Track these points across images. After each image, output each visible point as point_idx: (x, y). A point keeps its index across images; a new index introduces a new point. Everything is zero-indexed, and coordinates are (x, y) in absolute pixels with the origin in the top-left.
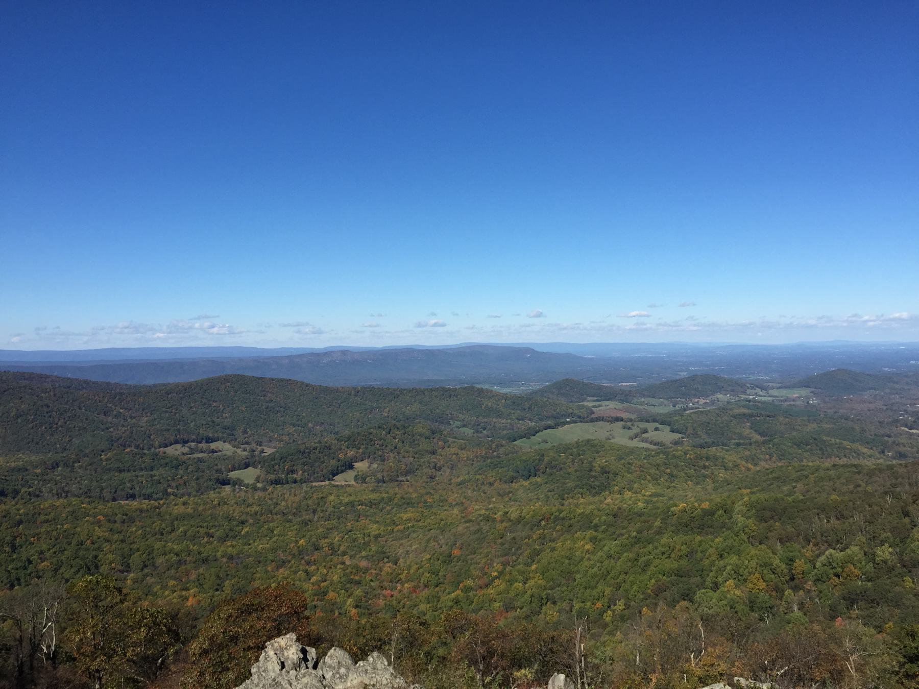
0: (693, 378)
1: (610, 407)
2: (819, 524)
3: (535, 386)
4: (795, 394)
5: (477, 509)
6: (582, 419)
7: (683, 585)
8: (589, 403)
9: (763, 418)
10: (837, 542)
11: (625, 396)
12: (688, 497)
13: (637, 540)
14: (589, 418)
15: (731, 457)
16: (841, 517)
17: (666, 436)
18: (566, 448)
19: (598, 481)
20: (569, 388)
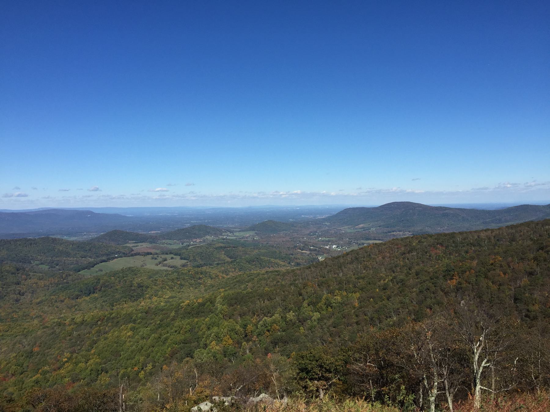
0: (193, 227)
1: (143, 247)
2: (260, 304)
3: (94, 235)
4: (247, 234)
5: (51, 319)
6: (125, 255)
7: (186, 349)
8: (130, 245)
9: (231, 249)
11: (153, 240)
12: (191, 296)
13: (160, 326)
14: (131, 254)
15: (214, 271)
16: (270, 299)
17: (178, 262)
18: (115, 274)
19: (136, 292)
20: (116, 236)
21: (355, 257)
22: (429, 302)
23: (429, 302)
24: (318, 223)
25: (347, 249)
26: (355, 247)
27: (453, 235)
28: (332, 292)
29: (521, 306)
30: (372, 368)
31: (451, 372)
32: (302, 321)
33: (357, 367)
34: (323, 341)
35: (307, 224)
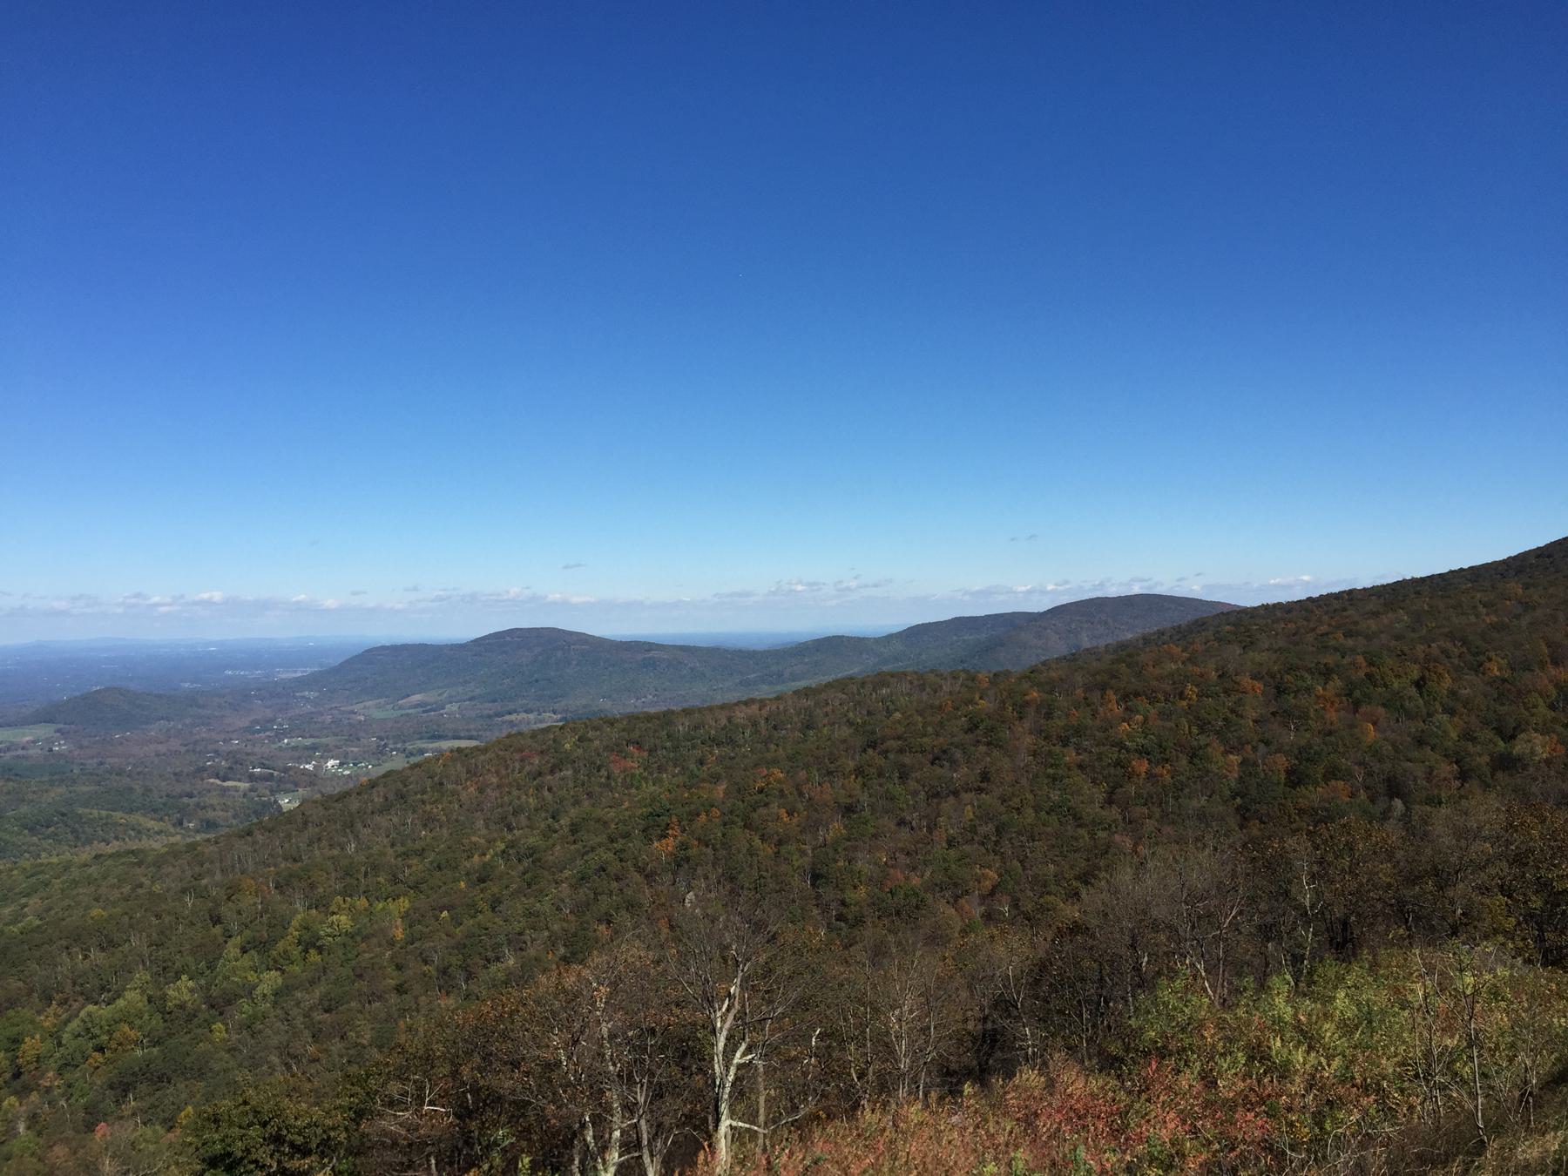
4: (25, 736)
10: (105, 990)
16: (109, 944)
21: (395, 791)
22: (605, 903)
23: (605, 903)
24: (279, 693)
25: (371, 769)
26: (397, 762)
27: (666, 718)
28: (322, 905)
29: (828, 893)
30: (437, 1116)
31: (658, 1094)
32: (219, 1005)
33: (392, 1123)
34: (290, 1057)
35: (241, 696)
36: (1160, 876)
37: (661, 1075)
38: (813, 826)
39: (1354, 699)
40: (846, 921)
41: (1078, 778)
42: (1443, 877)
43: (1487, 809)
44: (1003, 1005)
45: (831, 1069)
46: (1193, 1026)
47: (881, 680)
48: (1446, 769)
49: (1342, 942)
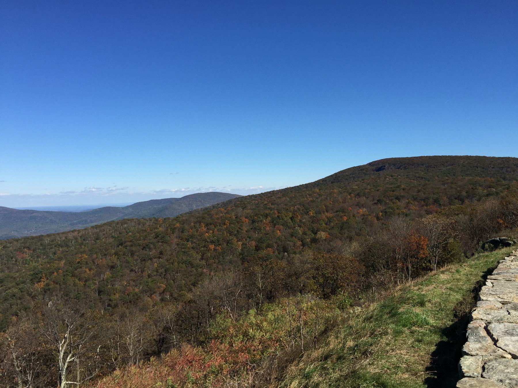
27: (40, 238)
29: (104, 297)
31: (37, 376)
36: (218, 281)
37: (38, 369)
38: (98, 274)
39: (274, 223)
40: (111, 306)
41: (192, 252)
42: (297, 275)
43: (309, 254)
44: (167, 329)
45: (105, 358)
46: (226, 329)
47: (124, 222)
48: (299, 243)
49: (270, 298)
